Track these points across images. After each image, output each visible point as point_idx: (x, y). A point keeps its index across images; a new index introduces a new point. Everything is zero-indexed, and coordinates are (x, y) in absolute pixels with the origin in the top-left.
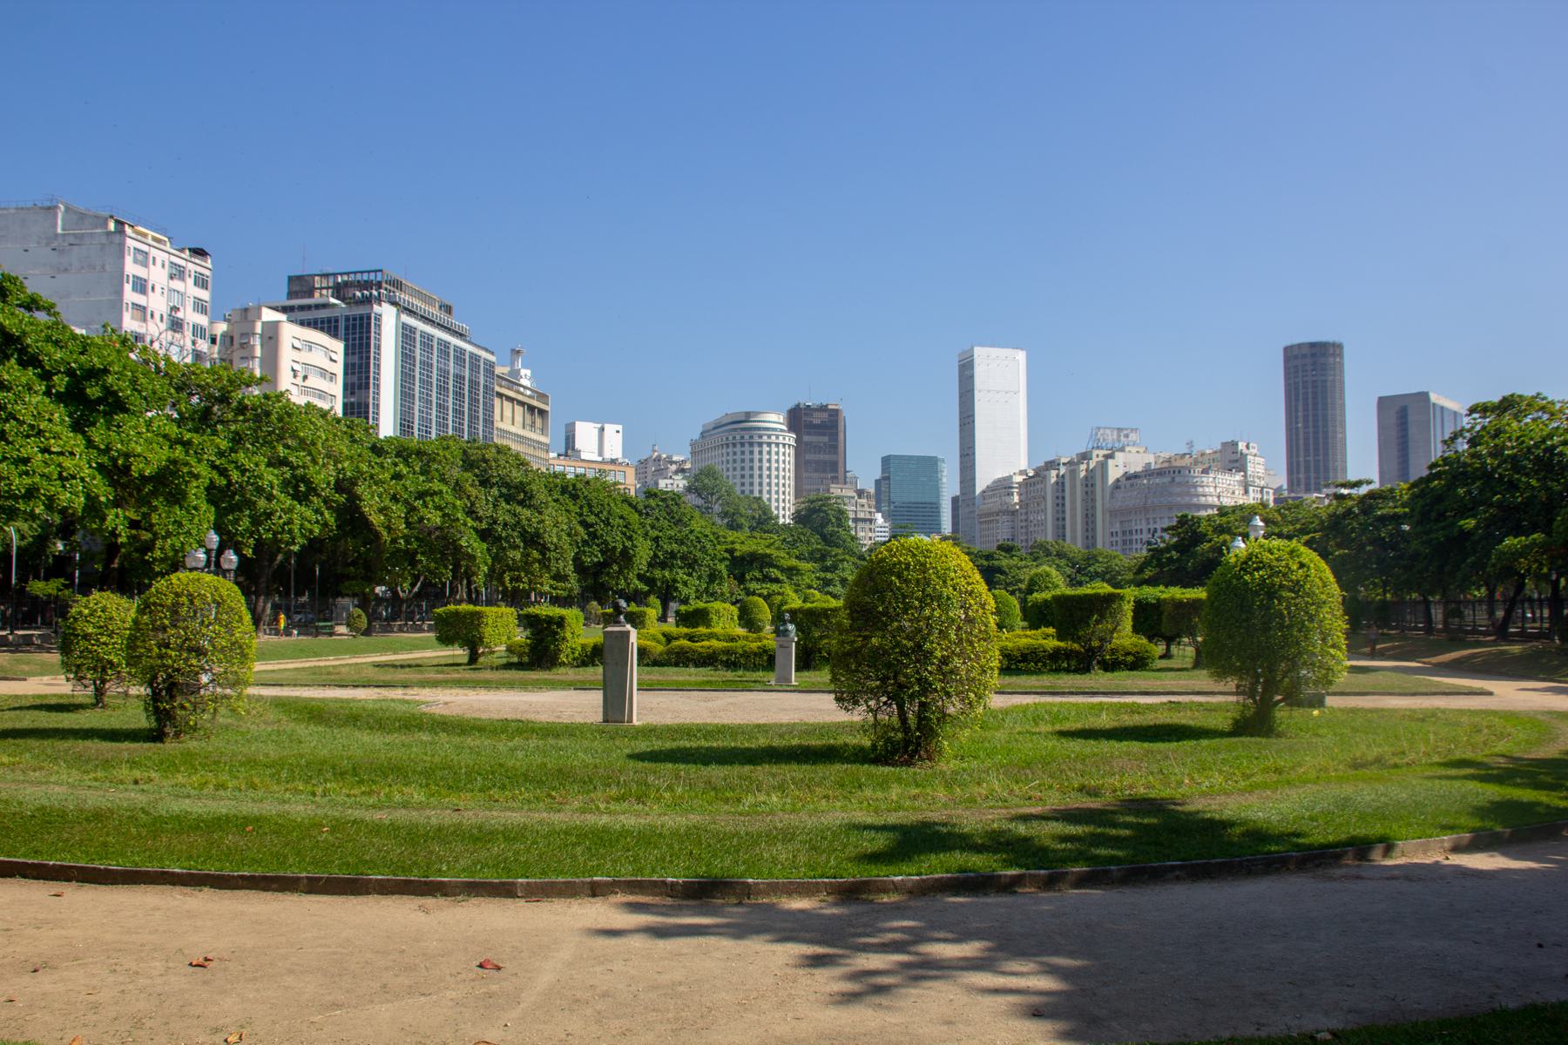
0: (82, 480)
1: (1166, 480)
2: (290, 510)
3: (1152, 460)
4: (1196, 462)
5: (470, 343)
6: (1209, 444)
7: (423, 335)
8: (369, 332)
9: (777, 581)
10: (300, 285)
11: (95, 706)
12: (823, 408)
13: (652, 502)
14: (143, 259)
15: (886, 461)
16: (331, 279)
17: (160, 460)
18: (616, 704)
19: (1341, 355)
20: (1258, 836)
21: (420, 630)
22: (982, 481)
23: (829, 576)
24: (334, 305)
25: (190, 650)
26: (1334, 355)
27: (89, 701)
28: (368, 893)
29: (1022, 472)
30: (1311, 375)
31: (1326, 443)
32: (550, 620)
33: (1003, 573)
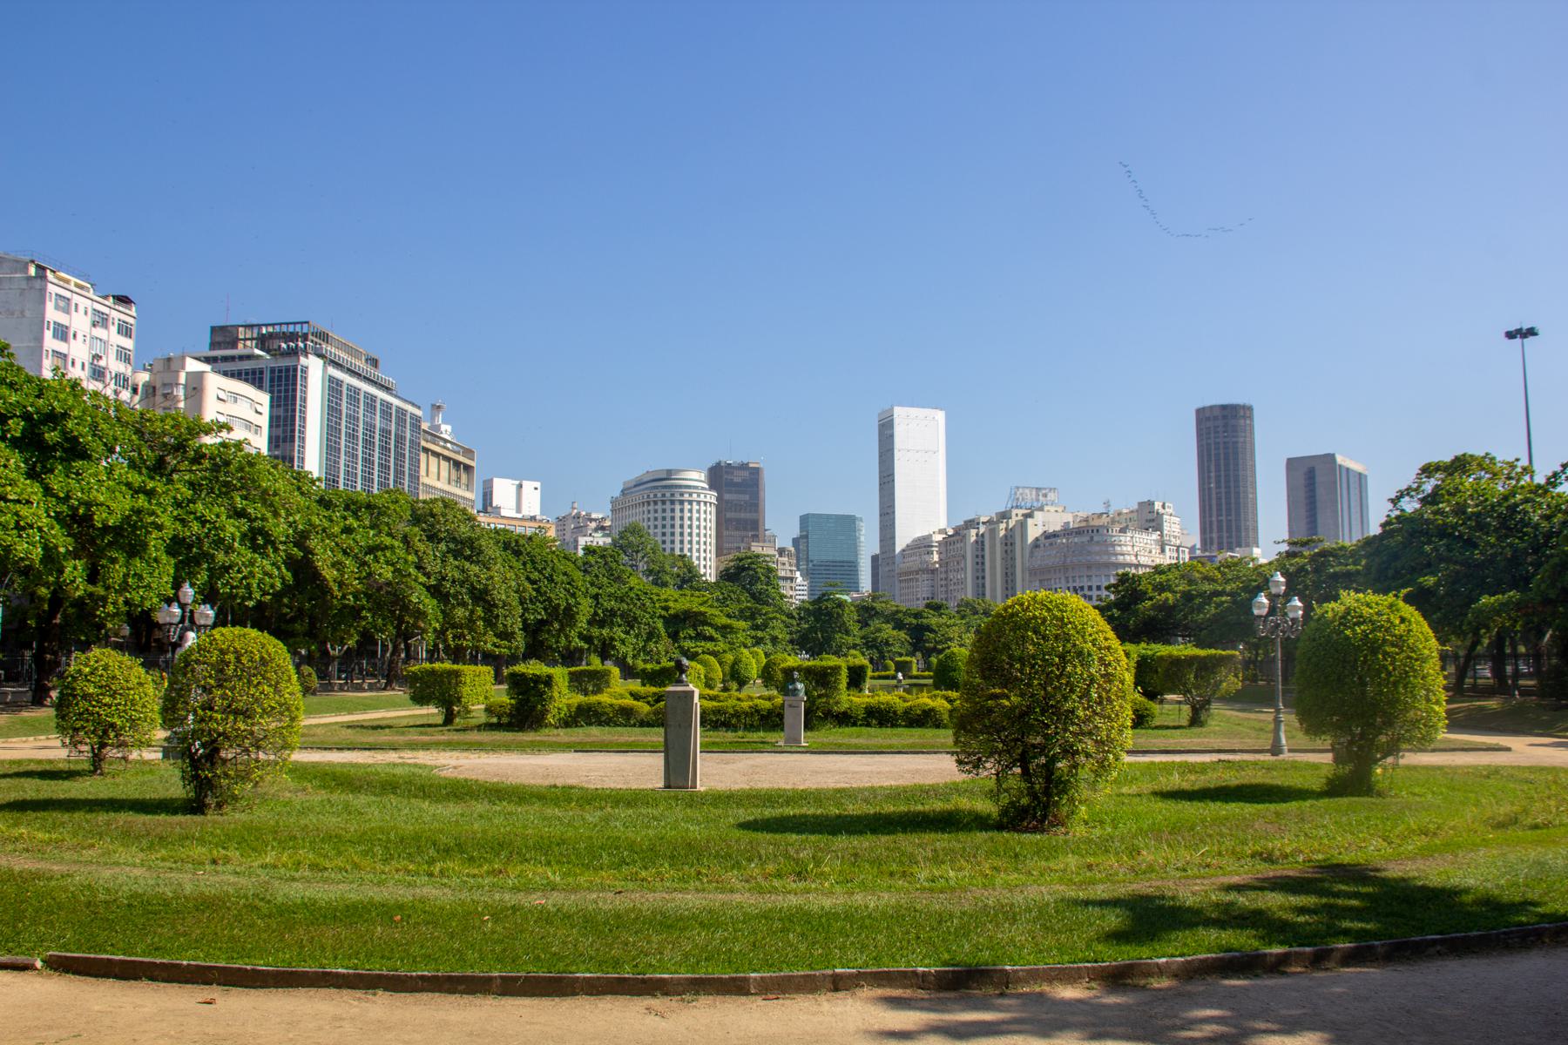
0: (40, 529)
1: (1085, 539)
2: (252, 563)
3: (1070, 519)
4: (1113, 521)
5: (396, 396)
6: (1126, 503)
7: (350, 387)
8: (295, 384)
9: (711, 639)
10: (223, 336)
11: (93, 772)
12: (744, 466)
13: (591, 559)
14: (65, 305)
15: (804, 520)
16: (256, 330)
17: (124, 509)
18: (678, 769)
19: (1251, 418)
20: (1493, 907)
21: (359, 688)
23: (760, 634)
24: (259, 357)
25: (236, 712)
26: (1244, 417)
27: (87, 766)
28: (574, 994)
29: (941, 532)
30: (1223, 437)
31: (1238, 503)
32: (537, 679)
33: (932, 631)
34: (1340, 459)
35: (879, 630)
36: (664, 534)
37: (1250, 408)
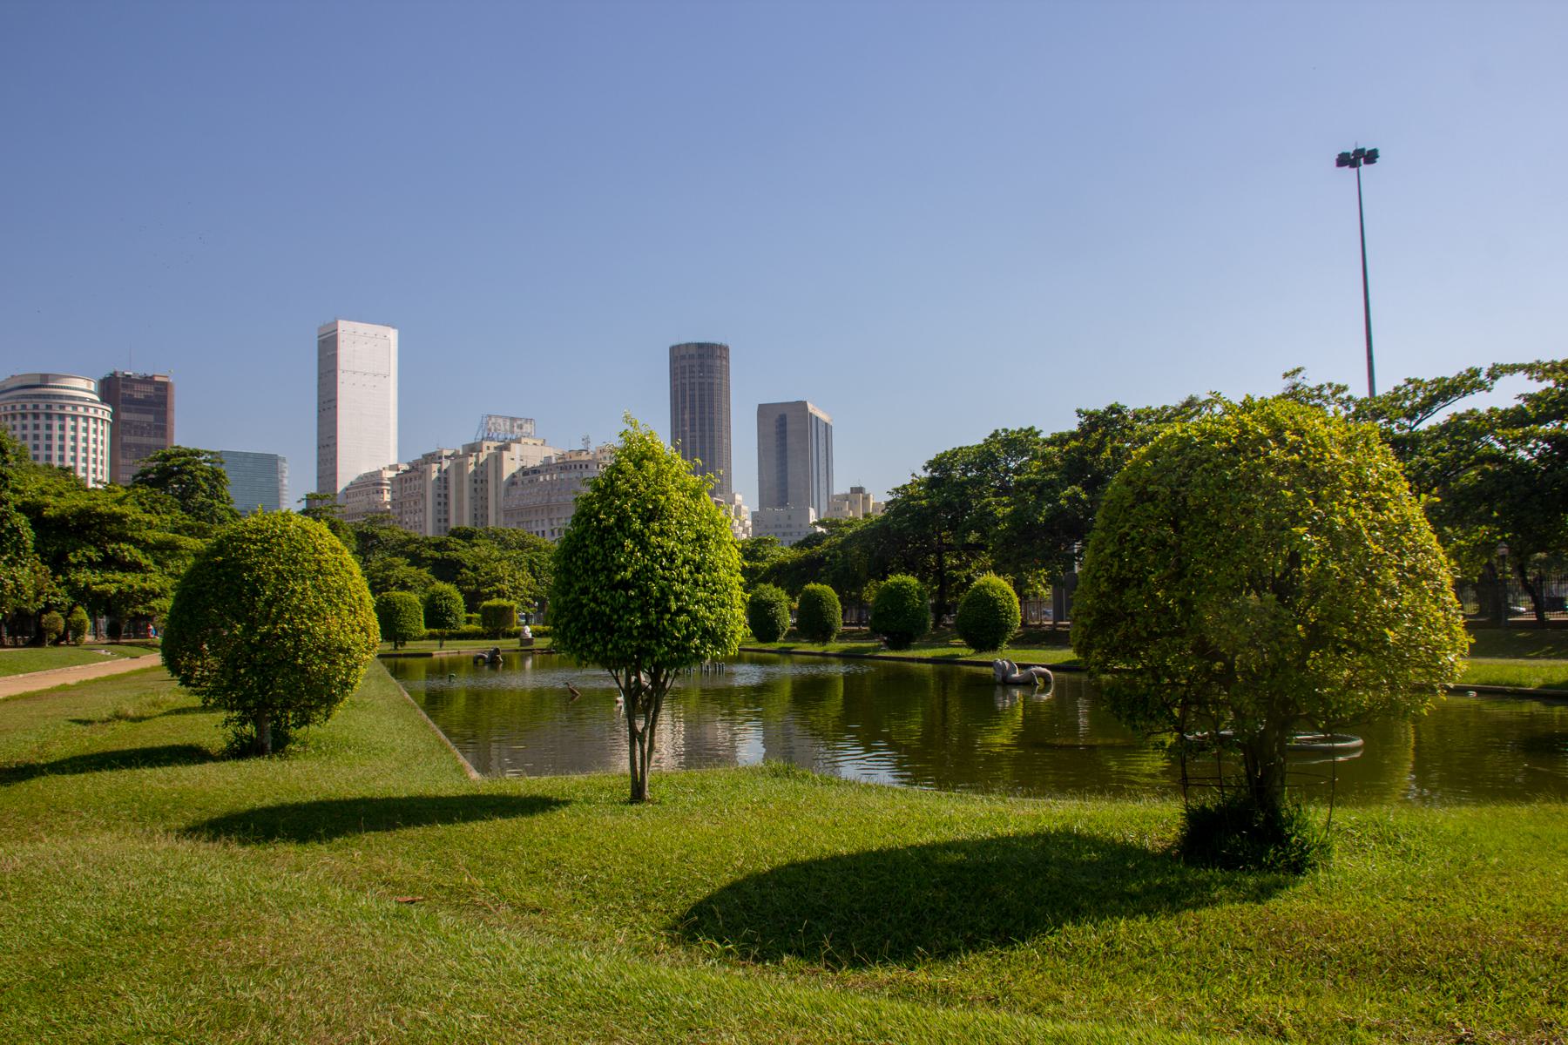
1: (573, 475)
9: (135, 567)
12: (147, 380)
22: (346, 476)
29: (392, 468)
30: (697, 376)
34: (810, 407)
35: (390, 567)
36: (36, 447)
37: (726, 349)
